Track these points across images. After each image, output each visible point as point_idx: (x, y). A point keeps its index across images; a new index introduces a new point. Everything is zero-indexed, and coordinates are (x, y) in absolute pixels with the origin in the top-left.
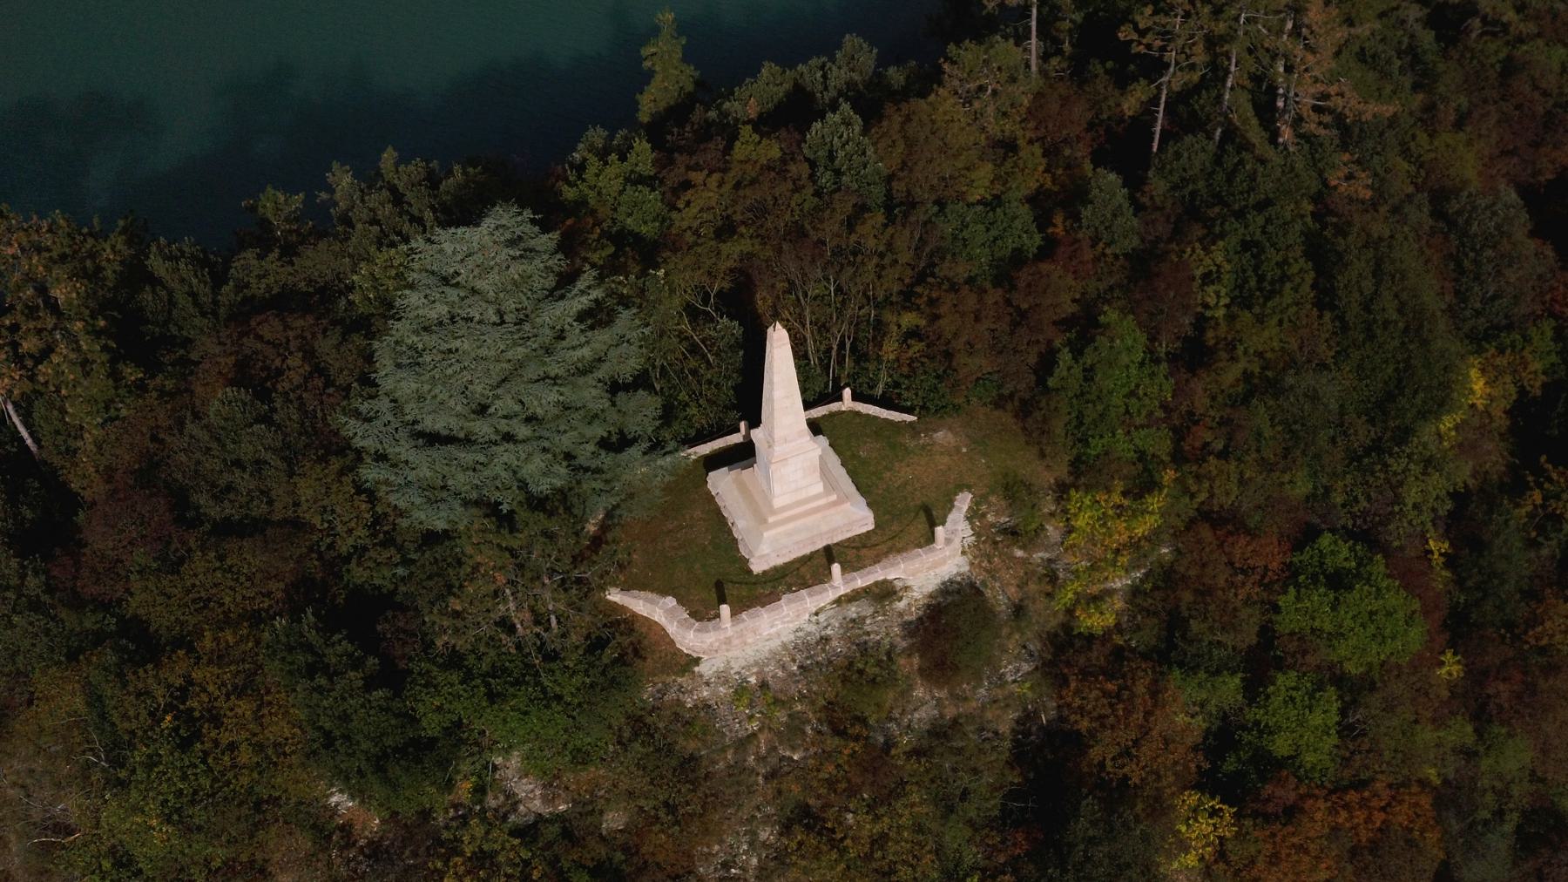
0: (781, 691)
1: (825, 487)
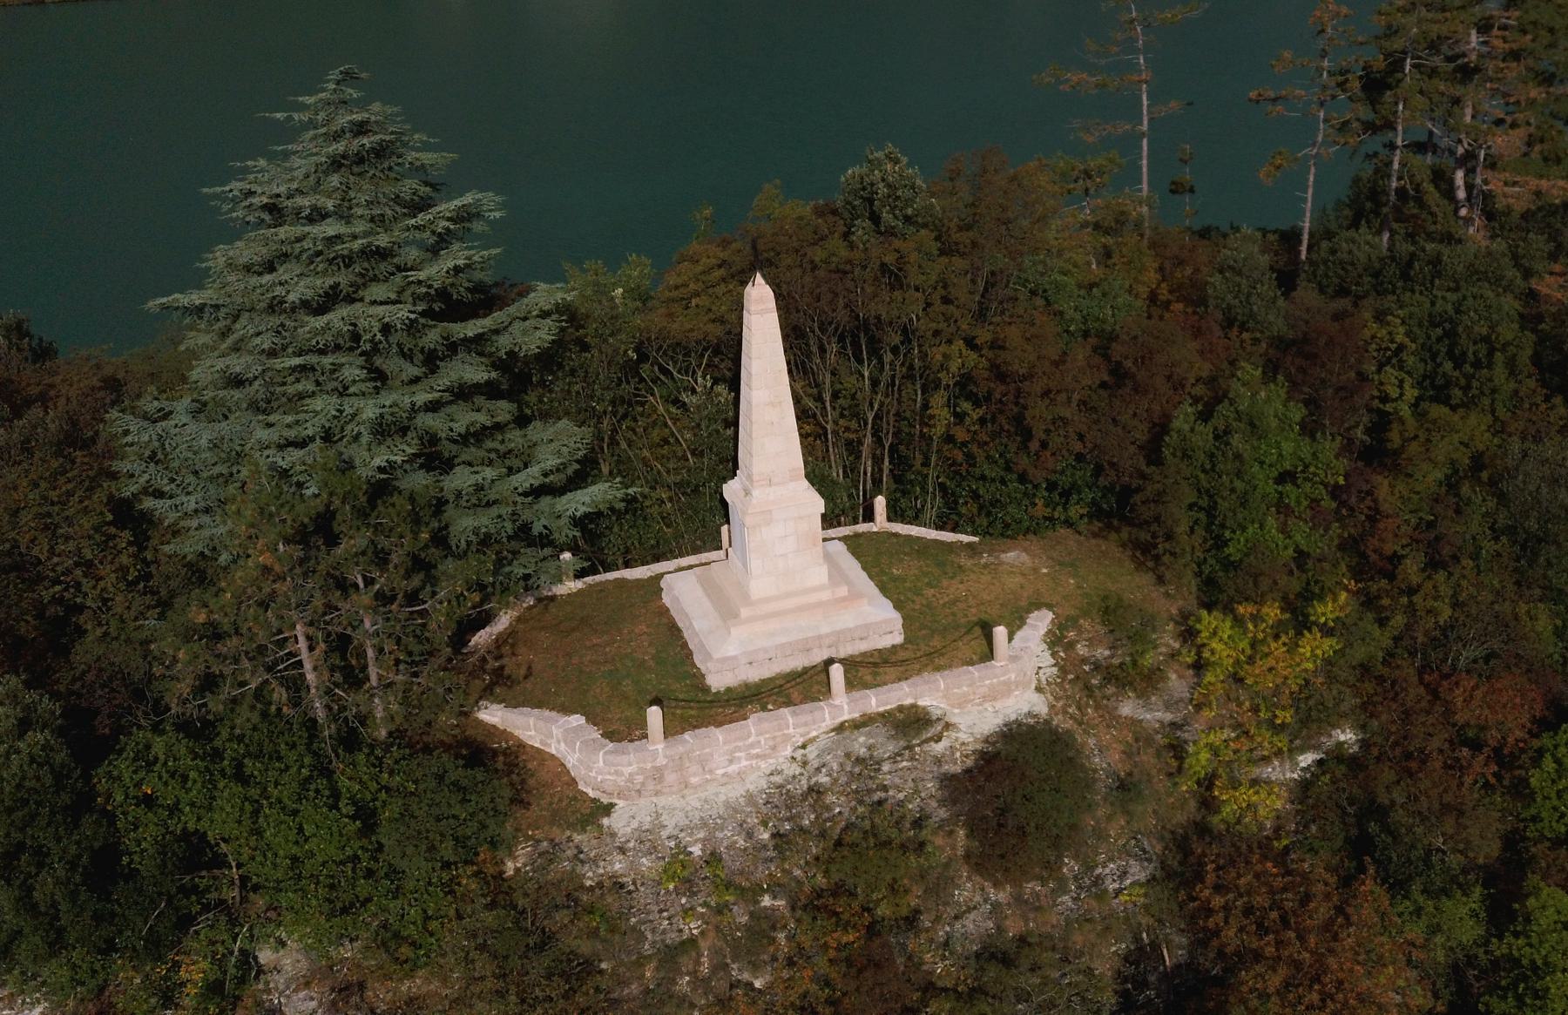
0: (742, 873)
1: (830, 576)
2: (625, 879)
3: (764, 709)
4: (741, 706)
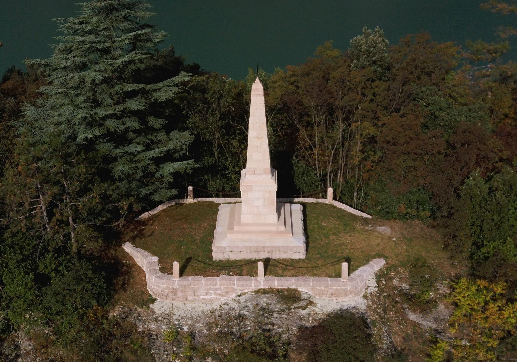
2: (154, 333)
3: (228, 274)
4: (220, 270)
